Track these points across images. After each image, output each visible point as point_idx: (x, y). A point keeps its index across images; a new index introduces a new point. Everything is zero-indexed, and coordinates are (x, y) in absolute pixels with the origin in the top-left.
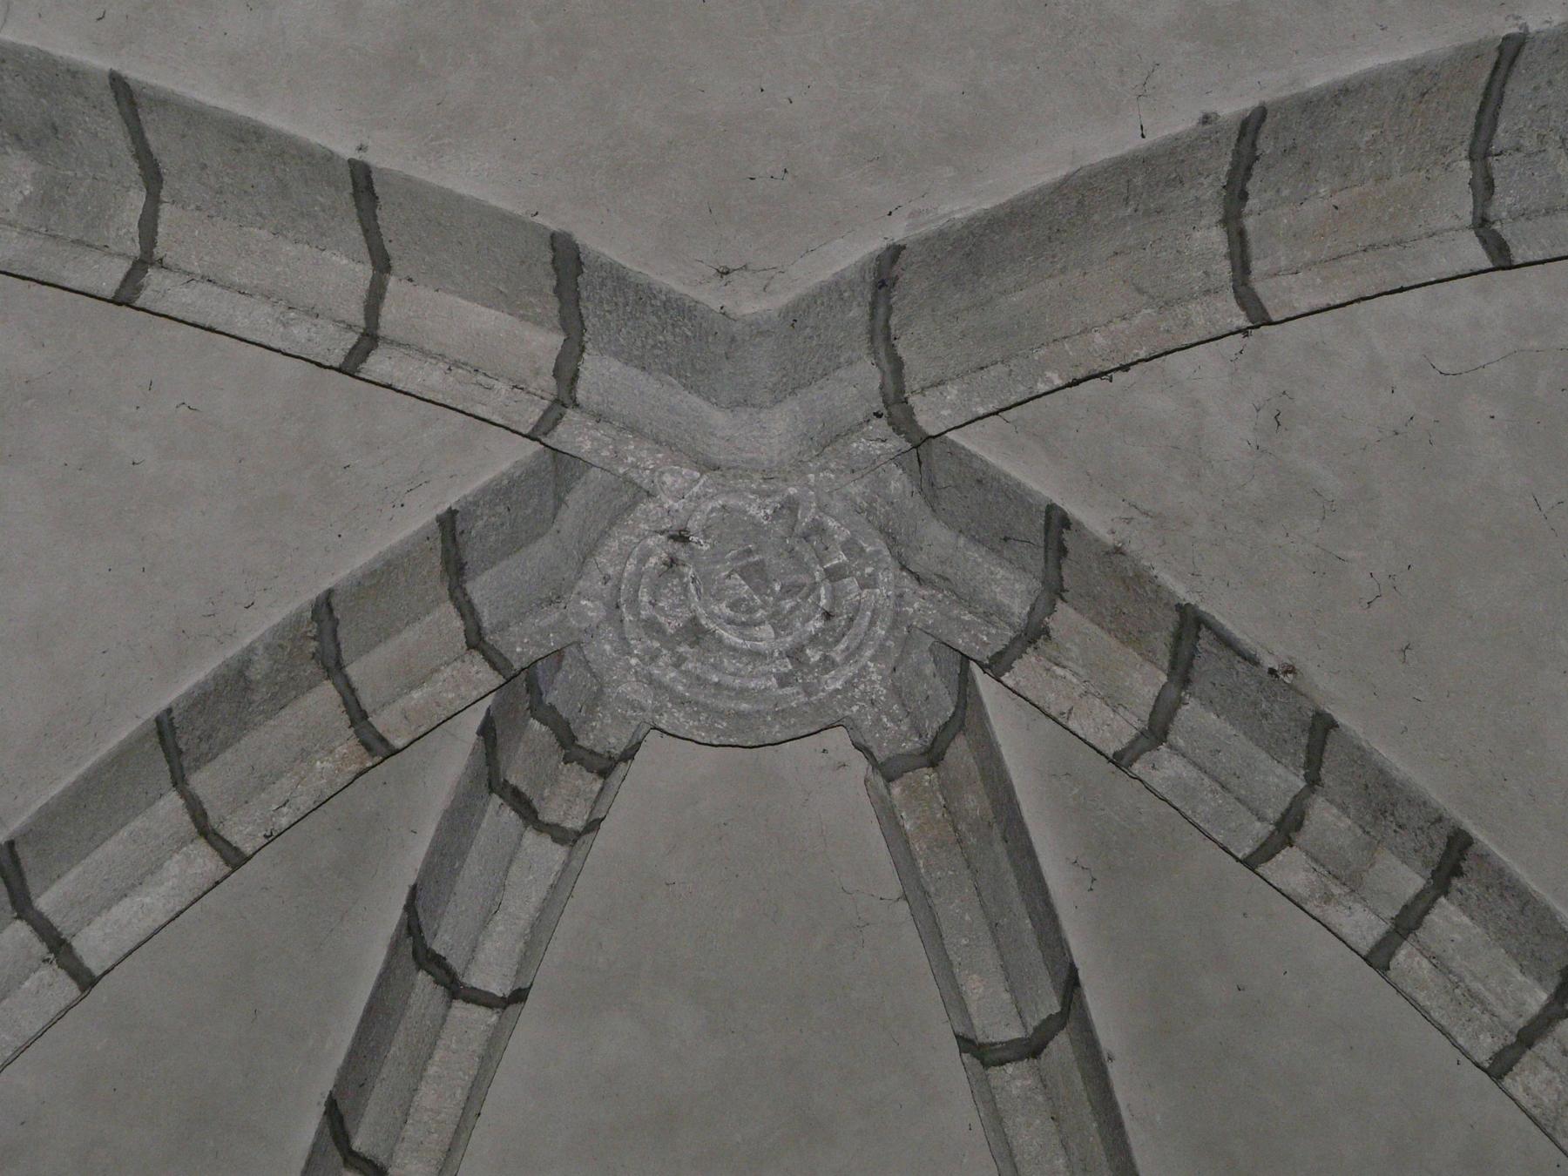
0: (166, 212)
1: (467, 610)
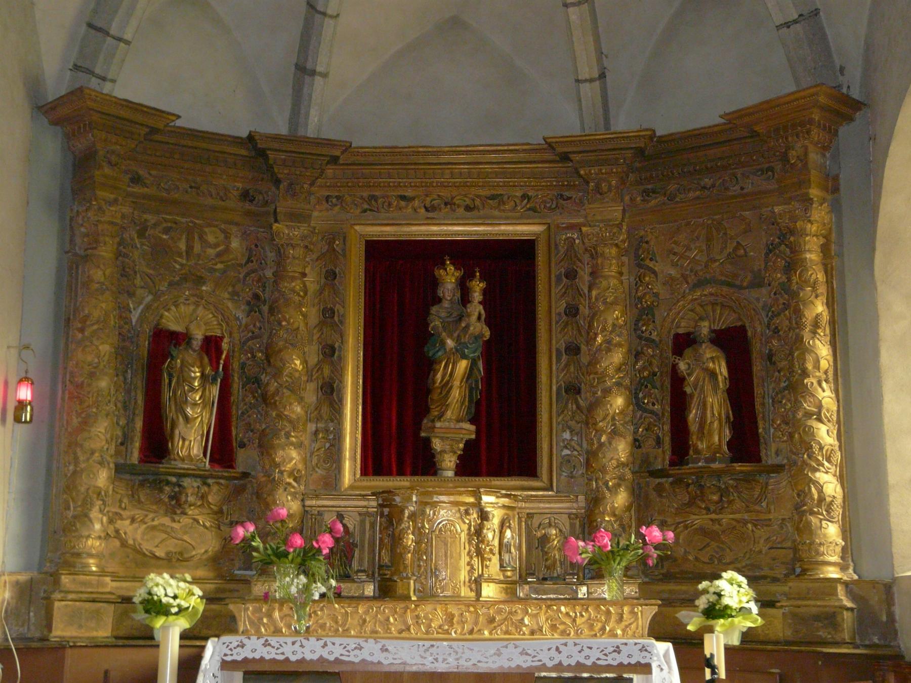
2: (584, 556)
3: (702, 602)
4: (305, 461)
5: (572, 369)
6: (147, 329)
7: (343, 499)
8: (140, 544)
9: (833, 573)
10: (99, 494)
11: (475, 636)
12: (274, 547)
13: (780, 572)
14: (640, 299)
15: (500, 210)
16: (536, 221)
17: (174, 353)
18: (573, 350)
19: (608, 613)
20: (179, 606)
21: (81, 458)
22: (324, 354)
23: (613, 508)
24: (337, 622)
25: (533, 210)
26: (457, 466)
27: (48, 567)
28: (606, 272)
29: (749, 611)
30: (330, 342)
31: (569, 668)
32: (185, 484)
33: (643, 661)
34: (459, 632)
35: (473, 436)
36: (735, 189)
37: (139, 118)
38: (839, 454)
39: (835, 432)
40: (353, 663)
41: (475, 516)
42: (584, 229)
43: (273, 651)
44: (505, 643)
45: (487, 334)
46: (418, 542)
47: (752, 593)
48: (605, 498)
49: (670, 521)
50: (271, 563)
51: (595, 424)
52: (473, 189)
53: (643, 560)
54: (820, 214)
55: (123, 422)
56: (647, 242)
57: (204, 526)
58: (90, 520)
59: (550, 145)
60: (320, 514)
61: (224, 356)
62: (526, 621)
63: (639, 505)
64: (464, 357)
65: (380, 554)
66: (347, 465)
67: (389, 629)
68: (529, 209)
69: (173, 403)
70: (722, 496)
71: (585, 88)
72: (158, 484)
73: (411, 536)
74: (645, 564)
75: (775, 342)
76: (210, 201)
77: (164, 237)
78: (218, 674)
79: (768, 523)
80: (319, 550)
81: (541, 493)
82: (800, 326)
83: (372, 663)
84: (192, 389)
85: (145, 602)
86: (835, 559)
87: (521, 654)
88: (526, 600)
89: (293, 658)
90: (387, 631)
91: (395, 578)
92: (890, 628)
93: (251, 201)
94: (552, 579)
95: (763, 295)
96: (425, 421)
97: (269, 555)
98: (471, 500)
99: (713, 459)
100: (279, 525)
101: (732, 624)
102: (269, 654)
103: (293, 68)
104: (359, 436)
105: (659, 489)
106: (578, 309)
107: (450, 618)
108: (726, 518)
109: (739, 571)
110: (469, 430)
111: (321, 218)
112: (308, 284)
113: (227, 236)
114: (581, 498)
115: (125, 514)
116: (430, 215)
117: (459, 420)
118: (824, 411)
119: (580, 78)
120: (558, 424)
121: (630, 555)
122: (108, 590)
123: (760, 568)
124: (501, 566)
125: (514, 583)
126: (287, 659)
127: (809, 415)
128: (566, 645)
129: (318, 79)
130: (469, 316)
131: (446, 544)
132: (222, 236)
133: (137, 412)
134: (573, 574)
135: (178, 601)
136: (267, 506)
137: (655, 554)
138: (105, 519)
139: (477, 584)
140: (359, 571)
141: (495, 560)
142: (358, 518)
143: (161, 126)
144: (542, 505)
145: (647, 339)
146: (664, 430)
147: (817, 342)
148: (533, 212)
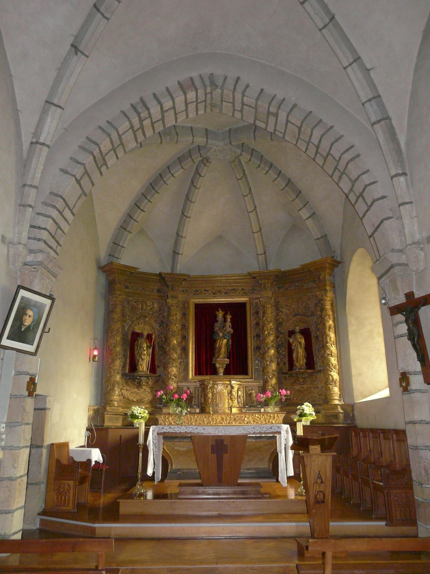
0: (178, 138)
1: (200, 154)
2: (263, 399)
3: (298, 412)
4: (177, 371)
5: (258, 342)
6: (130, 333)
7: (190, 383)
8: (129, 397)
9: (337, 402)
10: (117, 382)
11: (230, 424)
12: (169, 398)
13: (322, 402)
14: (278, 320)
15: (235, 294)
16: (246, 297)
17: (138, 340)
18: (258, 336)
19: (270, 416)
20: (141, 416)
21: (112, 372)
22: (183, 338)
23: (271, 384)
24: (188, 421)
25: (245, 293)
26: (224, 372)
27: (102, 404)
28: (267, 312)
29: (312, 414)
30: (184, 335)
31: (257, 433)
32: (142, 379)
33: (278, 431)
34: (225, 423)
35: (229, 363)
36: (305, 287)
37: (127, 269)
38: (338, 366)
39: (337, 360)
40: (195, 433)
41: (230, 387)
42: (261, 299)
43: (172, 430)
44: (238, 427)
45: (232, 331)
46: (212, 396)
47: (313, 409)
48: (269, 381)
49: (288, 387)
50: (168, 403)
51: (265, 358)
52: (227, 287)
53: (281, 400)
54: (330, 295)
55: (123, 360)
56: (280, 303)
57: (148, 392)
58: (115, 390)
59: (250, 274)
60: (182, 387)
61: (153, 340)
62: (246, 419)
63: (279, 383)
64: (225, 338)
65: (201, 399)
66: (190, 372)
67: (204, 422)
68: (244, 293)
69: (138, 354)
70: (304, 380)
71: (260, 257)
72: (133, 379)
73: (210, 394)
74: (282, 401)
75: (318, 333)
76: (148, 293)
77: (135, 304)
78: (156, 436)
79: (317, 388)
80: (183, 399)
81: (249, 380)
82: (325, 328)
83: (200, 433)
84: (144, 350)
85: (131, 415)
86: (337, 398)
87: (244, 430)
88: (245, 413)
89: (178, 432)
90: (204, 423)
91: (206, 407)
92: (353, 418)
93: (160, 292)
94: (253, 406)
95: (315, 318)
96: (214, 358)
97: (168, 401)
98: (228, 383)
99: (301, 369)
100: (170, 391)
101: (307, 418)
102: (171, 431)
103: (172, 252)
104: (194, 363)
105: (285, 378)
106: (259, 323)
107: (223, 419)
108: (305, 386)
109: (309, 402)
110: (227, 361)
111: (181, 297)
112: (178, 317)
113: (153, 303)
114: (261, 381)
115: (124, 388)
116: (214, 295)
117: (224, 358)
118: (333, 353)
119: (258, 254)
120: (254, 358)
121: (277, 398)
122: (120, 411)
123: (316, 401)
124: (238, 403)
125: (242, 408)
126: (176, 432)
127: (328, 355)
128: (256, 427)
129: (180, 256)
130: (226, 326)
131: (221, 396)
132: (152, 303)
133: (127, 357)
134: (260, 405)
135: (141, 415)
136: (167, 385)
137: (284, 398)
138: (119, 390)
139: (230, 408)
140: (194, 405)
141: (236, 401)
142: (194, 389)
143: (134, 271)
144: (249, 384)
145: (280, 332)
146: (286, 360)
147: (330, 333)
148: (245, 294)
